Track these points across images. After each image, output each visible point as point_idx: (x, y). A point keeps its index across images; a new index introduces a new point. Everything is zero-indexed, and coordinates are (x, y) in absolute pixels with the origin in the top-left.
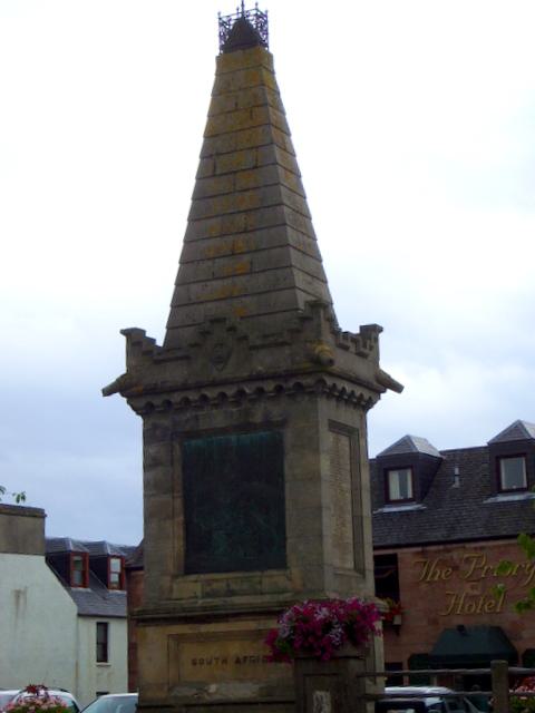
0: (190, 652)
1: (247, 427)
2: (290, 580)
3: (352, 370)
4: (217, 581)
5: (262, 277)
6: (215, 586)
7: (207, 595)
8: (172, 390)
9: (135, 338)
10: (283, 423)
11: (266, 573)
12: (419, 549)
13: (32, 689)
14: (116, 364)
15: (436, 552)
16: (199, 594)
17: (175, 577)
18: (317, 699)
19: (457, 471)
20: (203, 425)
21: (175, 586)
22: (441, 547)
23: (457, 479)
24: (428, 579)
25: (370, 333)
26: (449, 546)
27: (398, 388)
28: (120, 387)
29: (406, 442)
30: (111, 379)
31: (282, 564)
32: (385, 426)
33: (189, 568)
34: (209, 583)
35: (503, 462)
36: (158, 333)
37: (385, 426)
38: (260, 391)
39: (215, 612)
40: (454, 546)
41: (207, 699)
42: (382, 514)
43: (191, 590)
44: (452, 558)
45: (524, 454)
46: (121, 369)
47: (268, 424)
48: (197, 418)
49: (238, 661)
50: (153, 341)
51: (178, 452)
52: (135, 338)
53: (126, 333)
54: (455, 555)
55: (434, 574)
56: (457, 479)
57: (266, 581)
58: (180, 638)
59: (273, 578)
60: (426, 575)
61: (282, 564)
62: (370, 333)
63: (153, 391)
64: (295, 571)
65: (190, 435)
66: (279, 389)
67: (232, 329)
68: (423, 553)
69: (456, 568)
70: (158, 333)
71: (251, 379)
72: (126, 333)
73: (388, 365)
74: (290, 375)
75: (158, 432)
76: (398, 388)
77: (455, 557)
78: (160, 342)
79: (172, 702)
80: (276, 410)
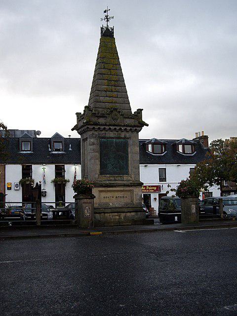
3: (137, 121)
5: (120, 99)
8: (102, 125)
9: (78, 114)
13: (70, 136)
25: (140, 111)
27: (147, 125)
31: (127, 173)
32: (144, 134)
37: (144, 134)
38: (126, 129)
47: (125, 138)
52: (78, 114)
53: (77, 114)
58: (101, 191)
59: (125, 177)
61: (127, 173)
62: (140, 111)
65: (103, 138)
66: (131, 130)
67: (119, 112)
72: (77, 114)
73: (145, 119)
76: (147, 125)
79: (99, 207)
80: (128, 135)
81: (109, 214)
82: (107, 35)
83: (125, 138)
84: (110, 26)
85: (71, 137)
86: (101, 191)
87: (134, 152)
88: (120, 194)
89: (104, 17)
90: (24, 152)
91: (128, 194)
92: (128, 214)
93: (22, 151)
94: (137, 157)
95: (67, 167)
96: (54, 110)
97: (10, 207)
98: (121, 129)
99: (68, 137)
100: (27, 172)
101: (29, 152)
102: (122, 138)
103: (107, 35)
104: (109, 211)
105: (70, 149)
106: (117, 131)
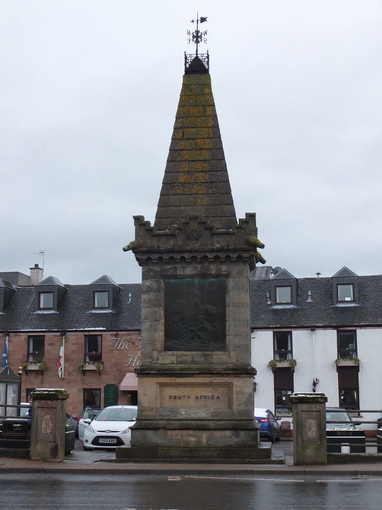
0: (170, 392)
1: (204, 275)
2: (230, 357)
4: (186, 355)
6: (184, 358)
7: (181, 363)
9: (139, 221)
10: (228, 275)
11: (214, 353)
12: (115, 333)
13: (318, 274)
14: (130, 235)
15: (123, 335)
16: (175, 362)
17: (160, 352)
18: (309, 424)
19: (130, 295)
20: (179, 272)
21: (160, 358)
22: (126, 333)
23: (130, 299)
24: (118, 348)
25: (251, 217)
26: (130, 332)
28: (133, 248)
29: (104, 278)
30: (126, 244)
31: (224, 348)
33: (167, 348)
34: (181, 356)
35: (96, 294)
36: (151, 217)
39: (174, 372)
40: (133, 332)
41: (180, 417)
42: (91, 313)
43: (169, 359)
44: (131, 338)
45: (292, 302)
46: (132, 238)
48: (175, 268)
49: (197, 398)
50: (148, 223)
51: (163, 285)
52: (139, 221)
54: (133, 337)
55: (122, 346)
56: (130, 299)
57: (215, 357)
58: (162, 385)
60: (117, 346)
62: (251, 217)
63: (151, 251)
64: (233, 354)
68: (117, 335)
69: (133, 343)
70: (151, 217)
71: (212, 251)
74: (234, 250)
75: (151, 274)
77: (133, 338)
78: (152, 225)
80: (224, 268)
81: (174, 432)
82: (197, 70)
83: (218, 275)
84: (203, 48)
85: (321, 276)
86: (162, 385)
87: (239, 301)
88: (208, 392)
89: (193, 30)
90: (46, 312)
91: (221, 392)
92: (218, 434)
93: (94, 308)
94: (246, 314)
95: (361, 334)
96: (88, 223)
97: (289, 413)
98: (206, 257)
99: (316, 276)
100: (282, 345)
101: (291, 306)
102: (210, 276)
103: (197, 70)
104: (177, 424)
105: (309, 300)
106: (200, 263)
